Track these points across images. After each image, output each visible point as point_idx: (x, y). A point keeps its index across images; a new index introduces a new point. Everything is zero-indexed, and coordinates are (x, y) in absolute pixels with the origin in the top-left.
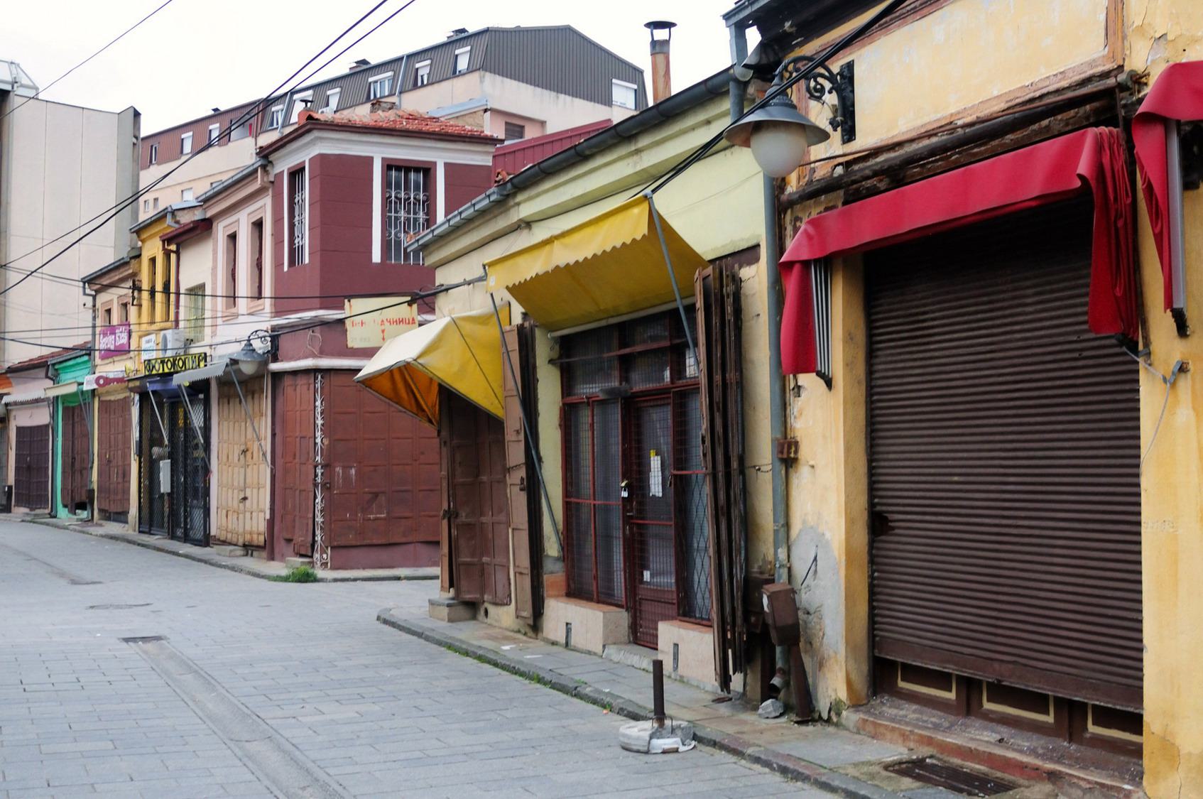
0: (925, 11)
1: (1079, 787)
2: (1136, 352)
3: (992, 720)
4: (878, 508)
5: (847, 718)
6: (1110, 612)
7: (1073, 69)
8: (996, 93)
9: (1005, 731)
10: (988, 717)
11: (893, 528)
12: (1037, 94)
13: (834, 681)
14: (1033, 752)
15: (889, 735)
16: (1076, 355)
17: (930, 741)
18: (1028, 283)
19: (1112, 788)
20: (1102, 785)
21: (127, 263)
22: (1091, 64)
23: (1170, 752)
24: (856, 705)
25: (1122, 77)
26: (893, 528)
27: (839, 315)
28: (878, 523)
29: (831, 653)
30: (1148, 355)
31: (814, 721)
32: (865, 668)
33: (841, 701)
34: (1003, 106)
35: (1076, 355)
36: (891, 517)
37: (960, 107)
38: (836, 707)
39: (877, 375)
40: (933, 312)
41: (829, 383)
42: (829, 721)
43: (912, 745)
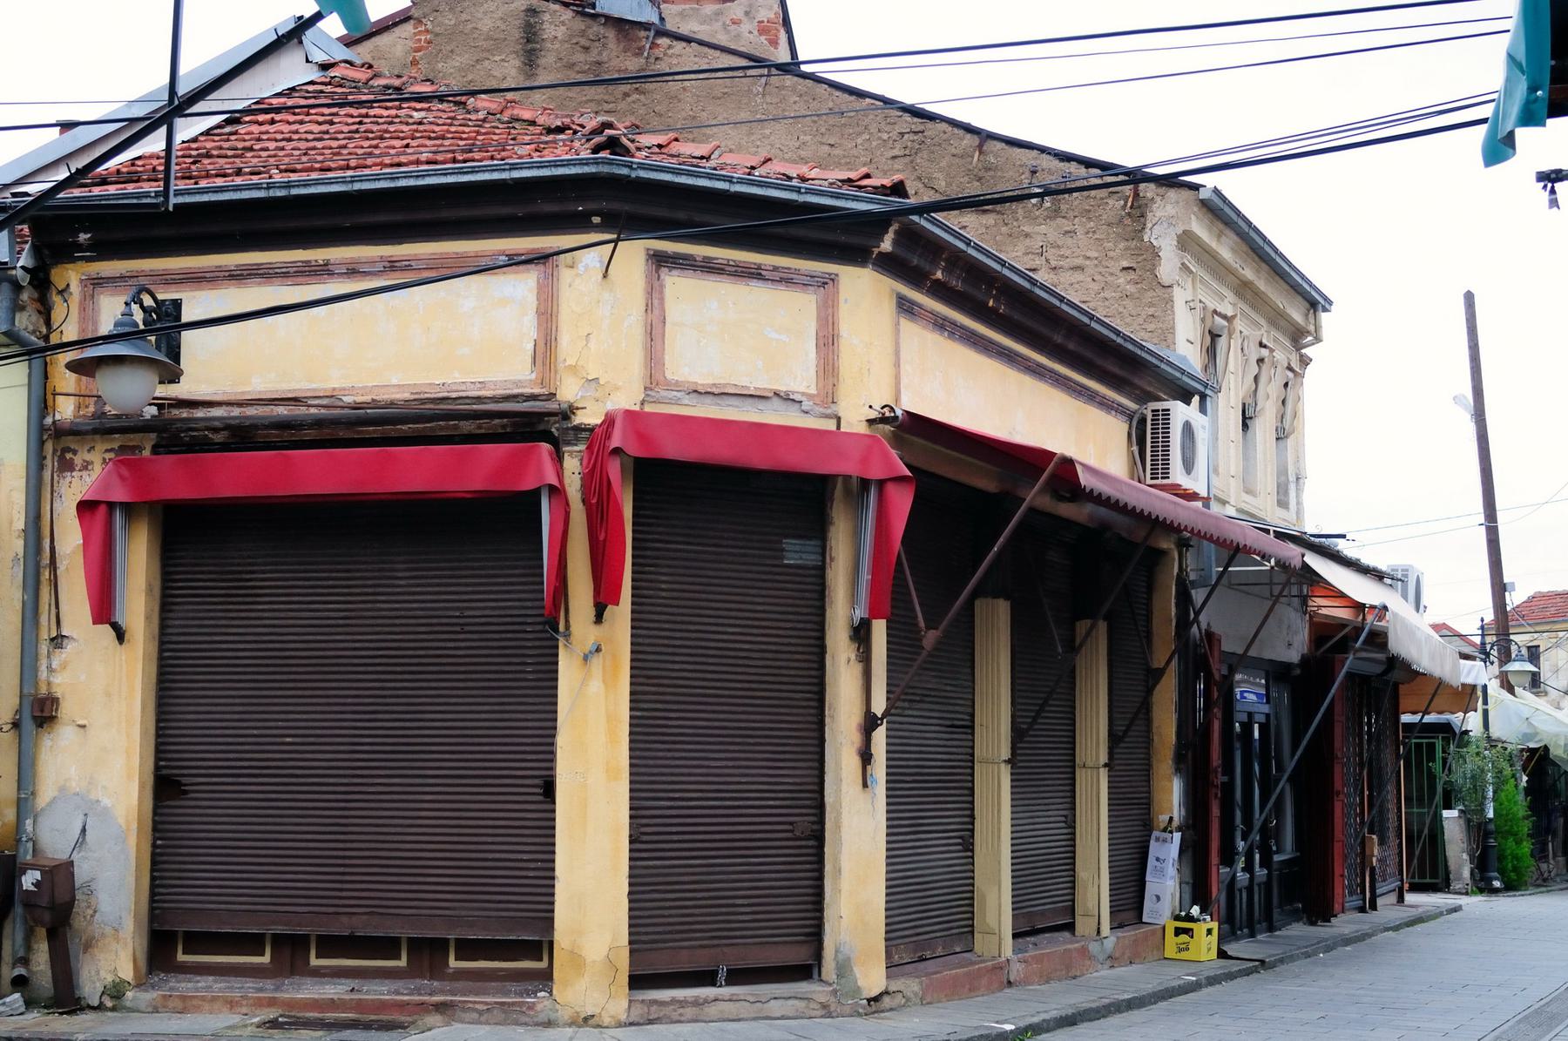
0: (300, 280)
1: (476, 1010)
2: (556, 630)
3: (324, 976)
4: (164, 772)
5: (134, 998)
6: (491, 856)
7: (495, 383)
8: (394, 381)
9: (355, 983)
10: (318, 973)
11: (186, 792)
12: (454, 395)
13: (114, 958)
14: (389, 993)
15: (207, 1006)
16: (458, 629)
17: (272, 1002)
18: (401, 558)
19: (513, 1004)
20: (503, 1004)
21: (1281, 436)
22: (517, 383)
23: (578, 962)
24: (139, 985)
25: (552, 406)
26: (186, 792)
27: (138, 560)
28: (167, 786)
29: (108, 930)
30: (567, 635)
31: (82, 1009)
32: (145, 943)
33: (123, 981)
34: (407, 396)
35: (458, 629)
36: (184, 780)
37: (346, 384)
38: (116, 992)
39: (170, 631)
40: (263, 572)
41: (120, 635)
42: (100, 1008)
43: (244, 1010)
